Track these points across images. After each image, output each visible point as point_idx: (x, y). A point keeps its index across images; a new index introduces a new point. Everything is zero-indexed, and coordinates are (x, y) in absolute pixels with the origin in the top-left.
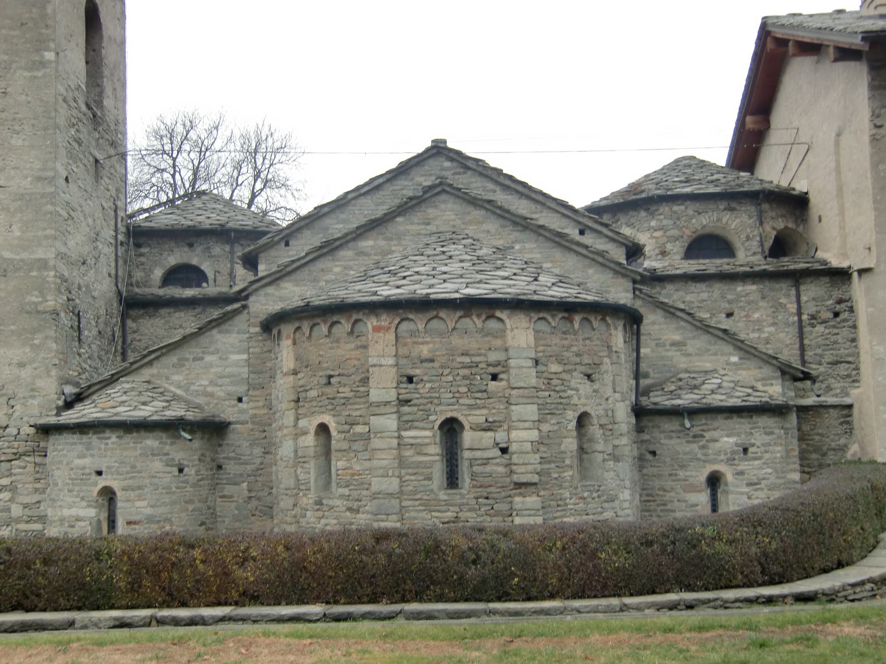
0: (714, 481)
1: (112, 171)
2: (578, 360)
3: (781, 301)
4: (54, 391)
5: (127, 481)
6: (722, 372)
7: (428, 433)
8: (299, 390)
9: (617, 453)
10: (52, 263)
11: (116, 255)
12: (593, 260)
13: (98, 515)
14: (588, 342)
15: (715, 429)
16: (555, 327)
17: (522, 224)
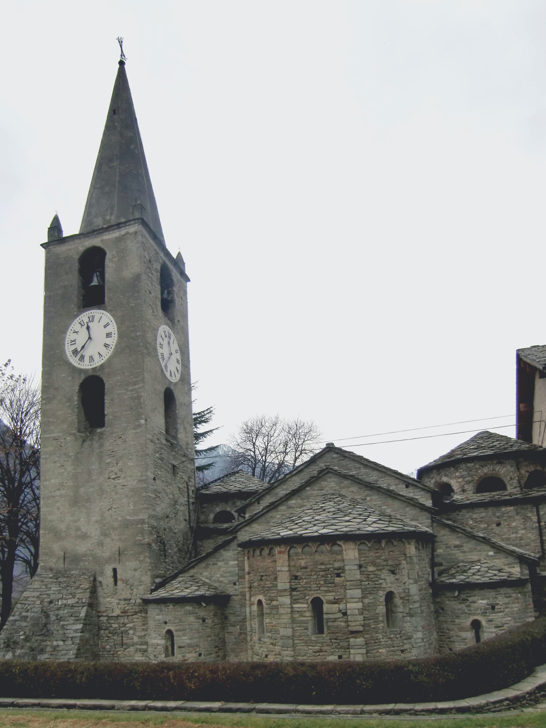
0: (476, 625)
1: (185, 469)
2: (385, 563)
3: (528, 515)
4: (149, 582)
5: (178, 627)
6: (484, 561)
7: (305, 605)
8: (251, 582)
9: (411, 612)
10: (146, 521)
11: (189, 509)
12: (409, 503)
13: (166, 643)
14: (391, 553)
15: (474, 596)
16: (370, 547)
17: (371, 487)
